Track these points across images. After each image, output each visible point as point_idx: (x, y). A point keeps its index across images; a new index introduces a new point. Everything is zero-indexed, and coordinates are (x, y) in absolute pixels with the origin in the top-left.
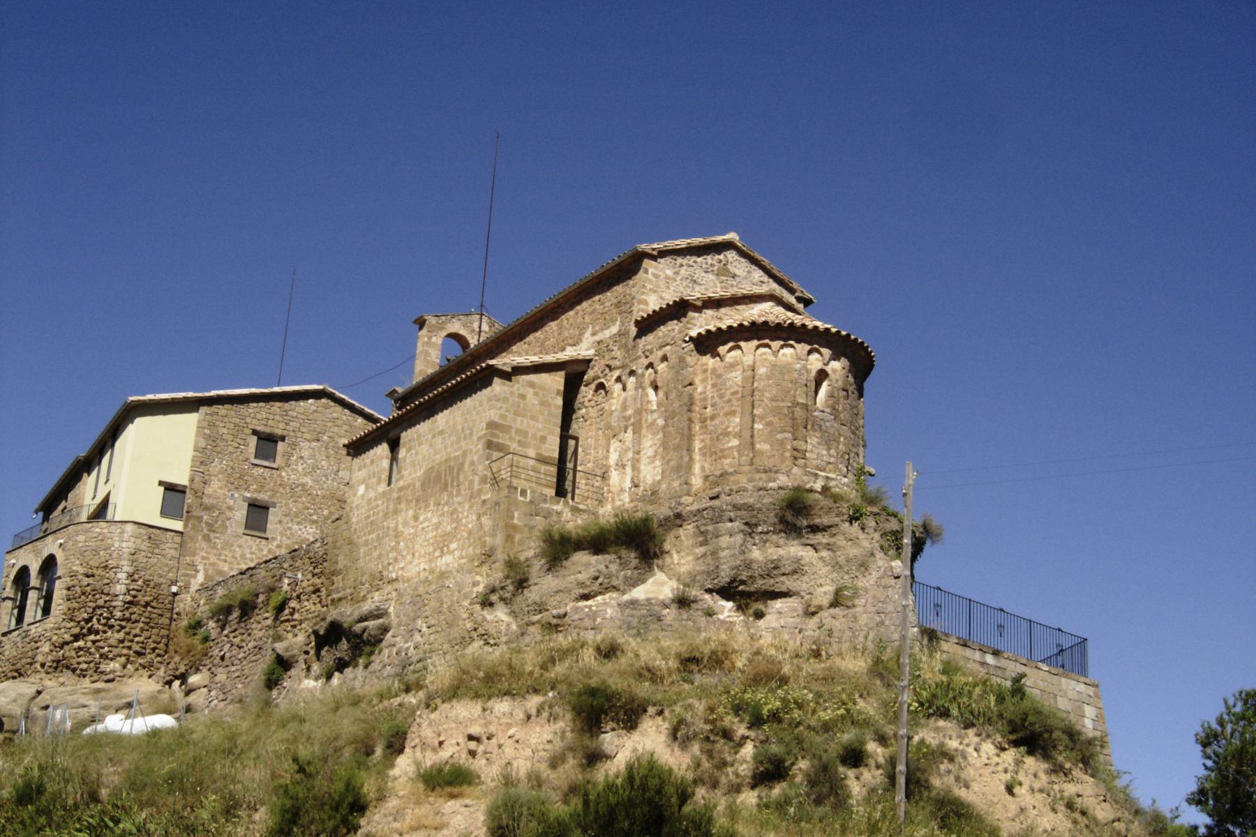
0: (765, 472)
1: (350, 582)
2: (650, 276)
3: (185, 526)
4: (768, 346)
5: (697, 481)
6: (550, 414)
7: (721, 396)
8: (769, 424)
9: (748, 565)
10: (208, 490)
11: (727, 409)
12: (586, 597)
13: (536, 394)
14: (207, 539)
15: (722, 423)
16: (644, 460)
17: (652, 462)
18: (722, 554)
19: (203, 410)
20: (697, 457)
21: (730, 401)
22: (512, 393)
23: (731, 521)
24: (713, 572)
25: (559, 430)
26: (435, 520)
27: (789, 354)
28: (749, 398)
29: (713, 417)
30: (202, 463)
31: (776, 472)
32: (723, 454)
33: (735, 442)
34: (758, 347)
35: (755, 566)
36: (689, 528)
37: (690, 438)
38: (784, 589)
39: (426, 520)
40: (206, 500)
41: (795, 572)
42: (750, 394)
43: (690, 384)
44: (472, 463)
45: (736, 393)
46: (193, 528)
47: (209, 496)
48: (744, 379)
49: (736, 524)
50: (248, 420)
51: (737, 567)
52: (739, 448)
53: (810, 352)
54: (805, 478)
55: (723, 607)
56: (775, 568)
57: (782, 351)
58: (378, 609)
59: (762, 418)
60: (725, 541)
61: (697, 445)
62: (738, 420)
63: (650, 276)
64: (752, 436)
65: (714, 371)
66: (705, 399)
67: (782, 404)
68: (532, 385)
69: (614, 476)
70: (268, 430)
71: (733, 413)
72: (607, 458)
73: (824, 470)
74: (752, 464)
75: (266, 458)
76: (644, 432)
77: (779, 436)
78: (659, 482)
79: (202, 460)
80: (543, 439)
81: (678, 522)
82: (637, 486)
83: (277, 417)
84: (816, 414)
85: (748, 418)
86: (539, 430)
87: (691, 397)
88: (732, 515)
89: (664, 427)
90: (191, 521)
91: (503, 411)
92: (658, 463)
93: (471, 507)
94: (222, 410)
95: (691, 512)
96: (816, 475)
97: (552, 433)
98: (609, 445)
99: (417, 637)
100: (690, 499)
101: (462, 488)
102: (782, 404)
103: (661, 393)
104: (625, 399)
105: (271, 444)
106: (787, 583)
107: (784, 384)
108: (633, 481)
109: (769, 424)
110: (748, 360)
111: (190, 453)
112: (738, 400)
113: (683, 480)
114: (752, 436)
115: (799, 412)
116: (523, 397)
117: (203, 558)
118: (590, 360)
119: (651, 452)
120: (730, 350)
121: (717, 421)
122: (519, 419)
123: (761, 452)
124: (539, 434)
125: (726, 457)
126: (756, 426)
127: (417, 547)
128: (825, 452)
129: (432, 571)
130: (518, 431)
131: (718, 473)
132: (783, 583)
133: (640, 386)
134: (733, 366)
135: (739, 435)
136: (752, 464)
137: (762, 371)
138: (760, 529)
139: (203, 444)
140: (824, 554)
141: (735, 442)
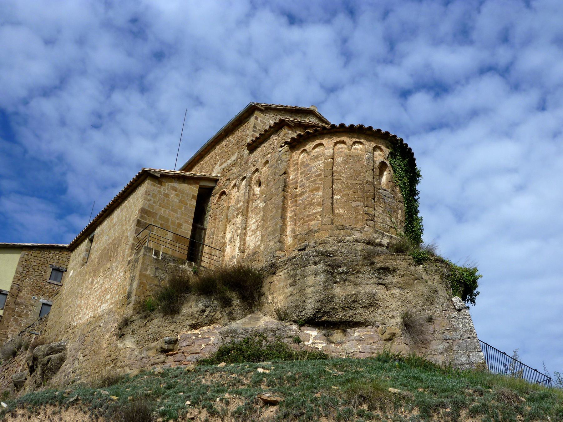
0: (343, 229)
1: (55, 332)
2: (259, 122)
3: (4, 313)
4: (343, 142)
5: (289, 240)
6: (186, 209)
7: (308, 179)
8: (346, 195)
9: (331, 299)
10: (20, 295)
11: (312, 186)
12: (194, 327)
13: (177, 195)
14: (16, 320)
15: (308, 197)
16: (249, 233)
17: (255, 233)
18: (309, 291)
19: (24, 252)
20: (289, 224)
21: (315, 181)
22: (159, 192)
23: (315, 264)
24: (300, 307)
25: (192, 221)
26: (101, 282)
27: (362, 148)
28: (330, 178)
29: (301, 194)
30: (19, 280)
31: (352, 229)
32: (310, 218)
33: (319, 209)
34: (336, 144)
35: (337, 300)
36: (281, 274)
37: (284, 209)
38: (361, 319)
39: (97, 282)
40: (18, 300)
41: (370, 305)
42: (331, 174)
43: (285, 173)
44: (127, 238)
45: (320, 175)
46: (8, 314)
47: (21, 298)
48: (326, 165)
49: (320, 266)
50: (49, 259)
51: (321, 301)
52: (321, 213)
53: (375, 149)
54: (375, 235)
55: (310, 335)
56: (354, 301)
57: (354, 147)
58: (60, 345)
59: (340, 191)
60: (311, 280)
61: (289, 214)
62: (321, 193)
63: (259, 122)
64: (332, 204)
65: (303, 163)
66: (297, 182)
67: (355, 182)
68: (175, 189)
69: (228, 249)
70: (58, 266)
71: (317, 189)
72: (224, 237)
73: (388, 232)
74: (332, 224)
75: (55, 280)
76: (250, 214)
77: (354, 204)
78: (259, 246)
79: (19, 278)
80: (179, 225)
81: (272, 270)
82: (243, 252)
83: (65, 259)
84: (381, 191)
85: (329, 191)
86: (177, 219)
87: (285, 181)
88: (317, 259)
89: (264, 208)
90: (8, 310)
91: (151, 202)
92: (258, 233)
93: (121, 268)
94: (34, 253)
95: (283, 261)
96: (383, 234)
97: (186, 222)
98: (225, 229)
99: (76, 364)
100: (283, 254)
101: (119, 256)
102: (355, 182)
103: (263, 186)
104: (238, 197)
105: (60, 274)
106: (362, 315)
107: (356, 168)
108: (240, 249)
109: (346, 195)
110: (329, 152)
111: (13, 274)
112: (321, 180)
113: (277, 239)
114: (332, 204)
115: (367, 187)
116: (167, 195)
117: (12, 331)
118: (218, 180)
119: (254, 227)
120: (315, 147)
121: (304, 197)
122: (163, 210)
123: (340, 215)
124: (177, 221)
125: (311, 220)
126: (335, 197)
127: (90, 301)
128: (388, 219)
129: (94, 317)
130: (161, 217)
131: (305, 232)
132: (360, 314)
133: (249, 185)
134: (317, 158)
135: (321, 204)
136: (332, 224)
137: (339, 159)
138: (340, 270)
139: (21, 270)
140: (396, 291)
141: (319, 209)
